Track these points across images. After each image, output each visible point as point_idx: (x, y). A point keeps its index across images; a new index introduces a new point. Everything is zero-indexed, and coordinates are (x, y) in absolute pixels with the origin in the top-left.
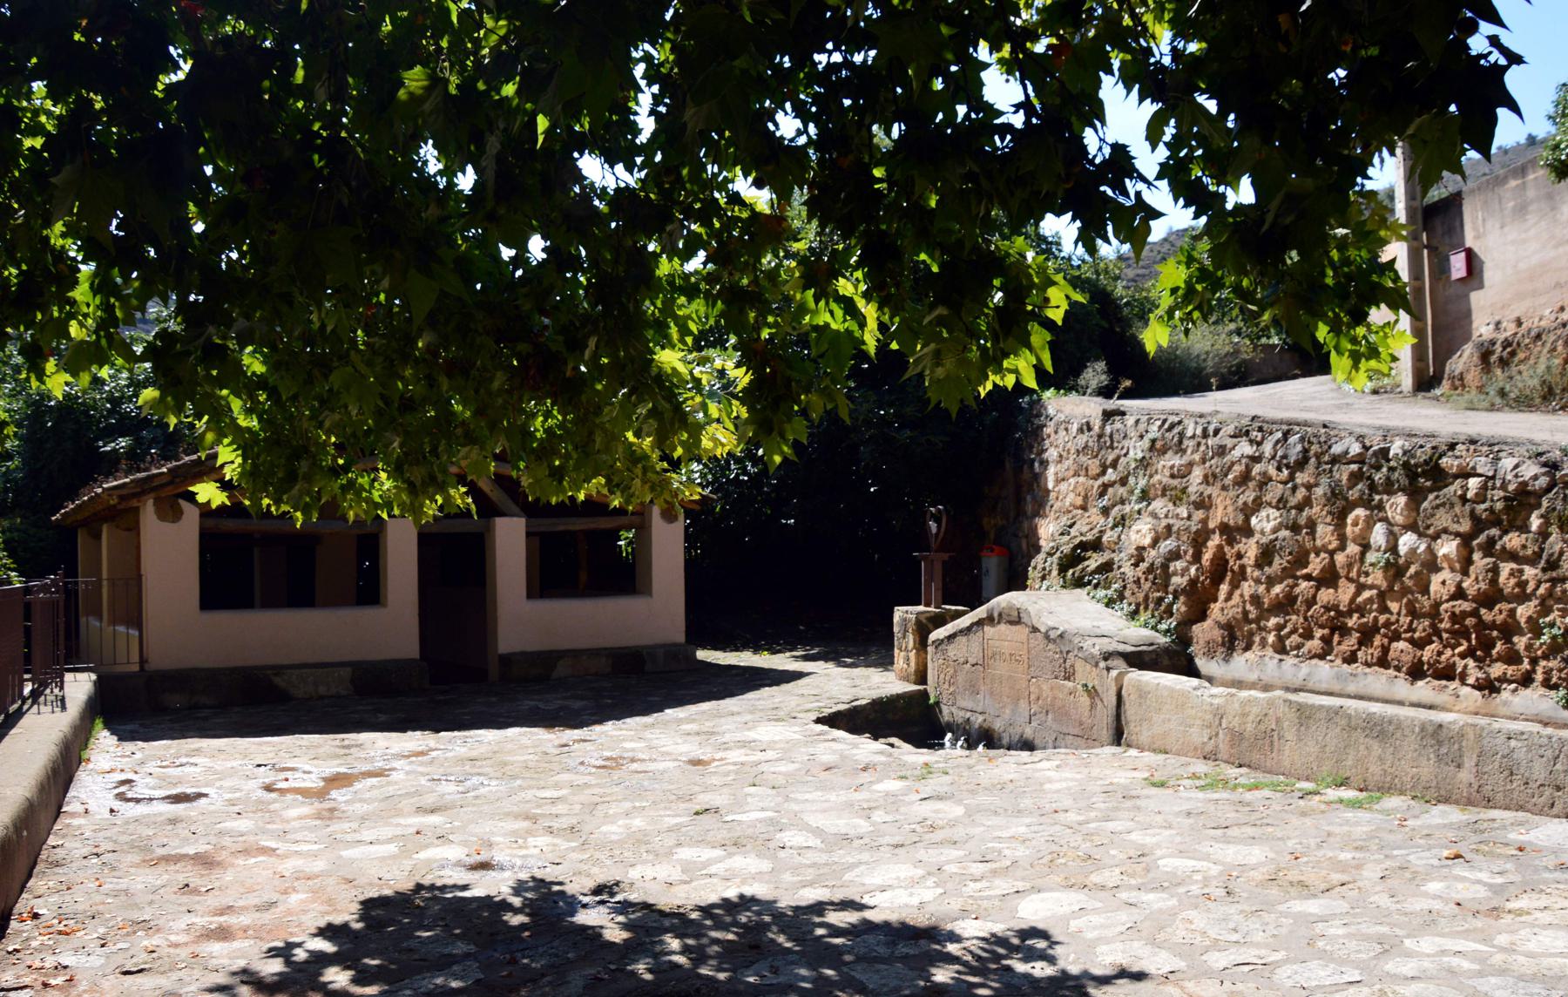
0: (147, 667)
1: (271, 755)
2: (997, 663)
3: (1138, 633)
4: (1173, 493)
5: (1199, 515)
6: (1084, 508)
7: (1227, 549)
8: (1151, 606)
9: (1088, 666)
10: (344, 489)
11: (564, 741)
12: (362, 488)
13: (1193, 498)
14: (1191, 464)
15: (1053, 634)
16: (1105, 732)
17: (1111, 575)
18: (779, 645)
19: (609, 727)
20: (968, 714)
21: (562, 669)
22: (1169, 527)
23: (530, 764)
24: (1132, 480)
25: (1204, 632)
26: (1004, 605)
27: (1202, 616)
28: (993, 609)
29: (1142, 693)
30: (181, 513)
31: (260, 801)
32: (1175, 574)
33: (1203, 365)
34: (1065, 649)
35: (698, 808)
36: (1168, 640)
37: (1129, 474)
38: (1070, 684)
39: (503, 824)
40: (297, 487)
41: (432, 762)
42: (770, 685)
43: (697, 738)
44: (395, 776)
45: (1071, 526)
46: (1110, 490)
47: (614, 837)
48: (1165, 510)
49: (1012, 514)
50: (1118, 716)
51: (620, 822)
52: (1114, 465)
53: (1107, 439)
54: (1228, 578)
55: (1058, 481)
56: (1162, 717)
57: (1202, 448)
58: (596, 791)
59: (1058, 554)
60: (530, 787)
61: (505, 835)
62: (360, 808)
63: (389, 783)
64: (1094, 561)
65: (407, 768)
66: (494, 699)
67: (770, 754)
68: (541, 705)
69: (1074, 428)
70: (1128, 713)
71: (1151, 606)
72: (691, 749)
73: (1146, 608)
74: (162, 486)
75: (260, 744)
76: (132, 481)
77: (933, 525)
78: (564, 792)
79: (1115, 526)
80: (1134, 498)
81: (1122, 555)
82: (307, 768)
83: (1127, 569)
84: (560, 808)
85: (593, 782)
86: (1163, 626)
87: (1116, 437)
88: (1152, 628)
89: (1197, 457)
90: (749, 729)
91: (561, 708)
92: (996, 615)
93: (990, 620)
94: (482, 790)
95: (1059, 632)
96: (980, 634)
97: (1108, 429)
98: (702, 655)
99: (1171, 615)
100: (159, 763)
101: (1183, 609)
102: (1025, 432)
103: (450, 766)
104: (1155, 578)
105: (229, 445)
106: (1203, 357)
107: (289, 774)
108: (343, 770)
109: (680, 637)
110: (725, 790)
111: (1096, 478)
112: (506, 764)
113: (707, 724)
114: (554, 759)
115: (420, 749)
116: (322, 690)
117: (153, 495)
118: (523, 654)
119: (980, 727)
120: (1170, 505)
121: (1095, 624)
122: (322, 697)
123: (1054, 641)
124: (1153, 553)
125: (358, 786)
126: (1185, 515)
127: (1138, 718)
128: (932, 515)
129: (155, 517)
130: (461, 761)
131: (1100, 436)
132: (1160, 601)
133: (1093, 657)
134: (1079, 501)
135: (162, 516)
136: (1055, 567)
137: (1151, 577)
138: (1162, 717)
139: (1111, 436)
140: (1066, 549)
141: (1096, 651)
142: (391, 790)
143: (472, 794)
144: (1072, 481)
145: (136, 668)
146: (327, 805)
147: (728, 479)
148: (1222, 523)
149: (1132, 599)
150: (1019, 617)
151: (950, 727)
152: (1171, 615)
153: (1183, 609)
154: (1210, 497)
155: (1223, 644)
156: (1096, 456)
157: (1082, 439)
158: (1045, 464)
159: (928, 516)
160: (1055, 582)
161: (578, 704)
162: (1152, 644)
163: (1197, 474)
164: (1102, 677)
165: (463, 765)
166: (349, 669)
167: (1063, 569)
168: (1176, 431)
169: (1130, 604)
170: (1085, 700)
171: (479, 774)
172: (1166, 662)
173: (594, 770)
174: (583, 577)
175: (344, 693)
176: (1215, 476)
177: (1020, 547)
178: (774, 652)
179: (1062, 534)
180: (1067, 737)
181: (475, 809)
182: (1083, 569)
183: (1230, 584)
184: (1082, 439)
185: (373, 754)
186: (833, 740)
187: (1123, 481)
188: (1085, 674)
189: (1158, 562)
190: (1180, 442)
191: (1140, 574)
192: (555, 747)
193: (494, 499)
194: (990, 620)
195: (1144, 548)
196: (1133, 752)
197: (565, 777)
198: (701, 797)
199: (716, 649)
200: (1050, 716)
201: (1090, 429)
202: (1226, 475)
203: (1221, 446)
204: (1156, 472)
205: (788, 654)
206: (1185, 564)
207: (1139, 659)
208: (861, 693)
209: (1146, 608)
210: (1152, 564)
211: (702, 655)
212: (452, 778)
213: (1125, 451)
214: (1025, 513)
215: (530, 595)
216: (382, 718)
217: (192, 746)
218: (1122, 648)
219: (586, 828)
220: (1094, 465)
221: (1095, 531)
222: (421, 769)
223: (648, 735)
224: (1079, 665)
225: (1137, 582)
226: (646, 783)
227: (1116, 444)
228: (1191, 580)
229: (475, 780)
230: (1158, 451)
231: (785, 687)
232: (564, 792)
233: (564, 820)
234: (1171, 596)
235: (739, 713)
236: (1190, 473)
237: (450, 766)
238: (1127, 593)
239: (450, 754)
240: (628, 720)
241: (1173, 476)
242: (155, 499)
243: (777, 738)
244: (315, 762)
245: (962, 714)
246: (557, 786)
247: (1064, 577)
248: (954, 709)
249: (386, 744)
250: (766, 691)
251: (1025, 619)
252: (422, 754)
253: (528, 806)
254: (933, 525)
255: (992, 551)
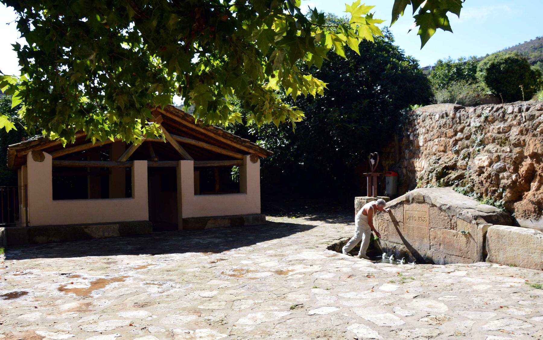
0: (29, 225)
1: (70, 268)
2: (411, 221)
3: (485, 207)
4: (500, 140)
5: (518, 149)
6: (445, 151)
7: (535, 165)
8: (489, 194)
9: (465, 223)
10: (88, 123)
11: (213, 260)
12: (98, 122)
13: (513, 142)
14: (510, 126)
15: (444, 208)
16: (475, 254)
17: (465, 180)
18: (299, 214)
19: (233, 253)
20: (395, 245)
21: (209, 225)
22: (499, 157)
23: (197, 274)
24: (473, 137)
25: (519, 206)
26: (415, 194)
27: (520, 198)
28: (409, 196)
29: (499, 236)
30: (44, 158)
31: (54, 299)
32: (503, 178)
33: (464, 101)
34: (451, 214)
35: (291, 304)
36: (501, 210)
37: (471, 134)
38: (454, 231)
39: (181, 317)
40: (56, 119)
41: (148, 272)
42: (301, 231)
43: (276, 258)
44: (128, 281)
45: (439, 160)
46: (460, 143)
47: (248, 329)
48: (495, 149)
49: (398, 159)
50: (484, 247)
51: (250, 316)
52: (462, 131)
53: (458, 119)
54: (537, 180)
55: (426, 141)
56: (513, 248)
57: (519, 118)
58: (232, 291)
59: (435, 172)
60: (197, 289)
61: (183, 326)
62: (105, 303)
63: (123, 286)
64: (453, 175)
65: (136, 276)
66: (180, 238)
67: (316, 268)
68: (201, 241)
69: (437, 117)
70: (490, 246)
71: (489, 194)
72: (274, 264)
73: (487, 195)
74: (36, 146)
75: (69, 261)
76: (22, 144)
77: (373, 161)
78: (215, 293)
79: (464, 159)
80: (475, 144)
81: (471, 171)
82: (86, 276)
83: (475, 177)
84: (213, 305)
85: (230, 286)
86: (498, 203)
87: (462, 118)
88: (491, 204)
89: (515, 122)
90: (299, 253)
91: (210, 243)
92: (411, 199)
93: (407, 201)
94: (172, 291)
95: (448, 207)
96: (402, 208)
97: (458, 115)
98: (269, 218)
99: (501, 198)
100: (15, 273)
101: (509, 195)
102: (404, 124)
103: (156, 275)
104: (492, 181)
105: (17, 96)
106: (464, 98)
107: (74, 280)
108: (103, 277)
109: (258, 210)
110: (301, 291)
111: (451, 137)
112: (184, 274)
113: (279, 250)
114: (209, 270)
115: (143, 264)
116: (106, 234)
117: (31, 150)
118: (193, 218)
119: (402, 250)
120: (498, 147)
121: (464, 203)
122: (106, 238)
123: (445, 211)
124: (489, 169)
125: (108, 287)
126: (508, 150)
127: (497, 248)
128: (372, 156)
129: (33, 160)
130: (162, 271)
131: (453, 119)
132: (494, 192)
133: (468, 218)
134: (442, 148)
135: (35, 159)
136: (434, 177)
137: (489, 180)
138: (513, 248)
139: (460, 118)
140: (439, 169)
141: (469, 215)
142: (123, 291)
143: (165, 293)
144: (436, 140)
145: (25, 225)
146: (87, 301)
147: (276, 146)
148: (533, 152)
149: (478, 191)
150: (424, 200)
151: (385, 250)
152: (501, 198)
153: (509, 195)
154: (524, 141)
155: (535, 212)
156: (452, 127)
157: (443, 121)
158: (417, 136)
159: (369, 157)
160: (434, 184)
161: (217, 241)
162: (494, 212)
163: (515, 131)
164: (474, 228)
165: (163, 274)
166: (118, 225)
167: (438, 178)
168: (500, 111)
169: (477, 194)
170: (463, 239)
171: (171, 280)
172: (502, 220)
173: (229, 278)
174: (217, 187)
175: (115, 235)
176: (527, 130)
177: (402, 172)
178: (297, 217)
179: (435, 163)
180: (452, 256)
181: (166, 305)
182: (448, 178)
183: (539, 182)
184: (443, 121)
185: (120, 267)
186: (342, 259)
187: (468, 138)
188: (462, 226)
189: (493, 173)
190: (504, 116)
191: (483, 179)
192: (208, 263)
193: (180, 152)
194: (407, 201)
195: (483, 167)
196: (495, 265)
197: (215, 282)
198: (290, 296)
199: (272, 216)
200: (442, 246)
201: (447, 116)
202: (535, 129)
203: (532, 115)
204: (489, 132)
205: (303, 218)
206: (509, 174)
207: (491, 219)
208: (343, 235)
209: (487, 195)
210: (490, 174)
211: (269, 218)
212: (156, 283)
213: (468, 124)
214: (405, 158)
215: (196, 194)
216: (130, 247)
217: (37, 263)
218: (481, 214)
219: (231, 321)
220: (450, 132)
221: (453, 161)
222: (142, 277)
223: (252, 256)
224: (459, 222)
225: (481, 183)
226: (258, 286)
227: (462, 121)
228: (513, 181)
229: (169, 284)
230: (489, 122)
231: (306, 232)
232: (215, 293)
233: (216, 313)
234: (501, 189)
235: (291, 245)
236: (510, 130)
237: (156, 275)
238: (475, 188)
239: (158, 267)
240: (241, 248)
241: (499, 133)
242: (32, 151)
243: (315, 258)
244: (91, 272)
245: (392, 244)
246: (211, 289)
247: (439, 182)
248: (387, 242)
249: (128, 262)
250: (299, 234)
251: (427, 200)
252: (144, 267)
253: (196, 303)
254: (373, 161)
255: (390, 174)
